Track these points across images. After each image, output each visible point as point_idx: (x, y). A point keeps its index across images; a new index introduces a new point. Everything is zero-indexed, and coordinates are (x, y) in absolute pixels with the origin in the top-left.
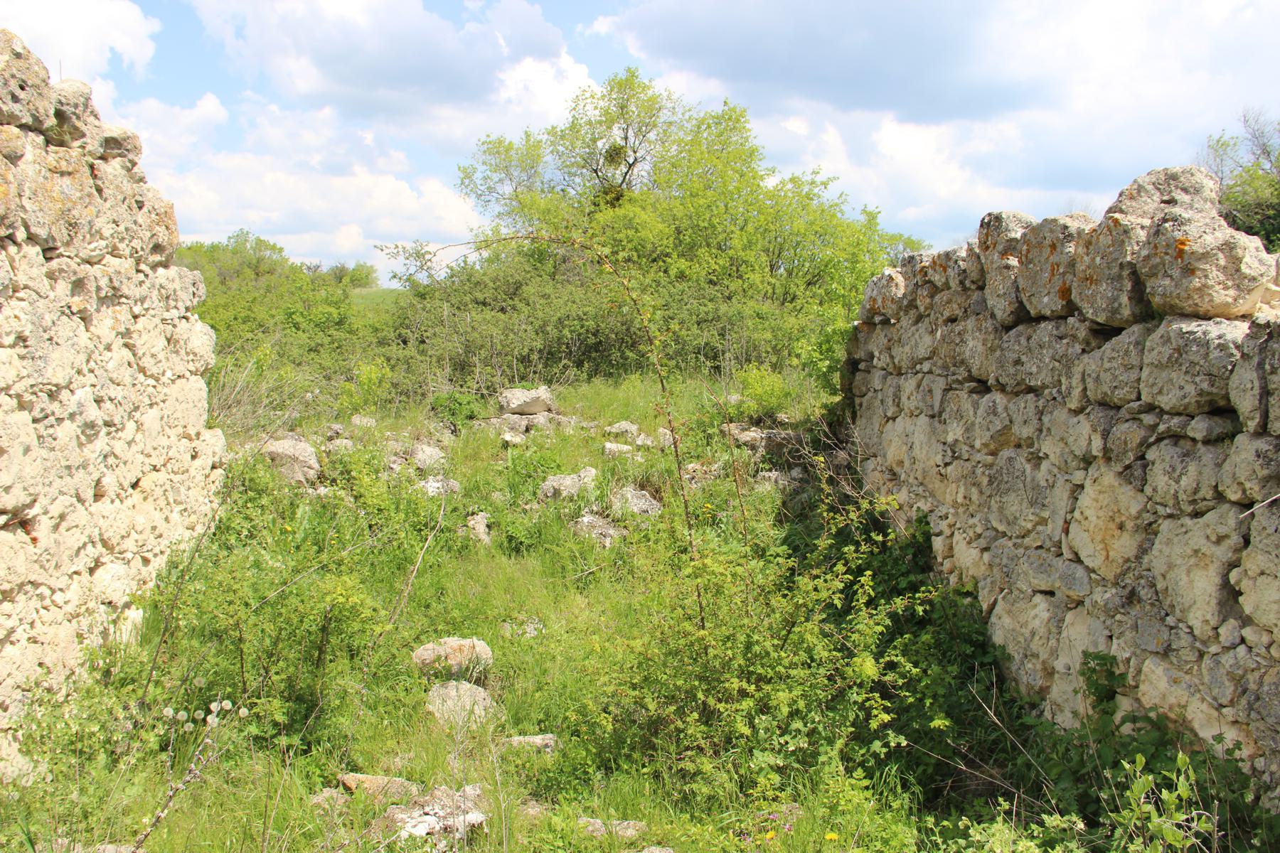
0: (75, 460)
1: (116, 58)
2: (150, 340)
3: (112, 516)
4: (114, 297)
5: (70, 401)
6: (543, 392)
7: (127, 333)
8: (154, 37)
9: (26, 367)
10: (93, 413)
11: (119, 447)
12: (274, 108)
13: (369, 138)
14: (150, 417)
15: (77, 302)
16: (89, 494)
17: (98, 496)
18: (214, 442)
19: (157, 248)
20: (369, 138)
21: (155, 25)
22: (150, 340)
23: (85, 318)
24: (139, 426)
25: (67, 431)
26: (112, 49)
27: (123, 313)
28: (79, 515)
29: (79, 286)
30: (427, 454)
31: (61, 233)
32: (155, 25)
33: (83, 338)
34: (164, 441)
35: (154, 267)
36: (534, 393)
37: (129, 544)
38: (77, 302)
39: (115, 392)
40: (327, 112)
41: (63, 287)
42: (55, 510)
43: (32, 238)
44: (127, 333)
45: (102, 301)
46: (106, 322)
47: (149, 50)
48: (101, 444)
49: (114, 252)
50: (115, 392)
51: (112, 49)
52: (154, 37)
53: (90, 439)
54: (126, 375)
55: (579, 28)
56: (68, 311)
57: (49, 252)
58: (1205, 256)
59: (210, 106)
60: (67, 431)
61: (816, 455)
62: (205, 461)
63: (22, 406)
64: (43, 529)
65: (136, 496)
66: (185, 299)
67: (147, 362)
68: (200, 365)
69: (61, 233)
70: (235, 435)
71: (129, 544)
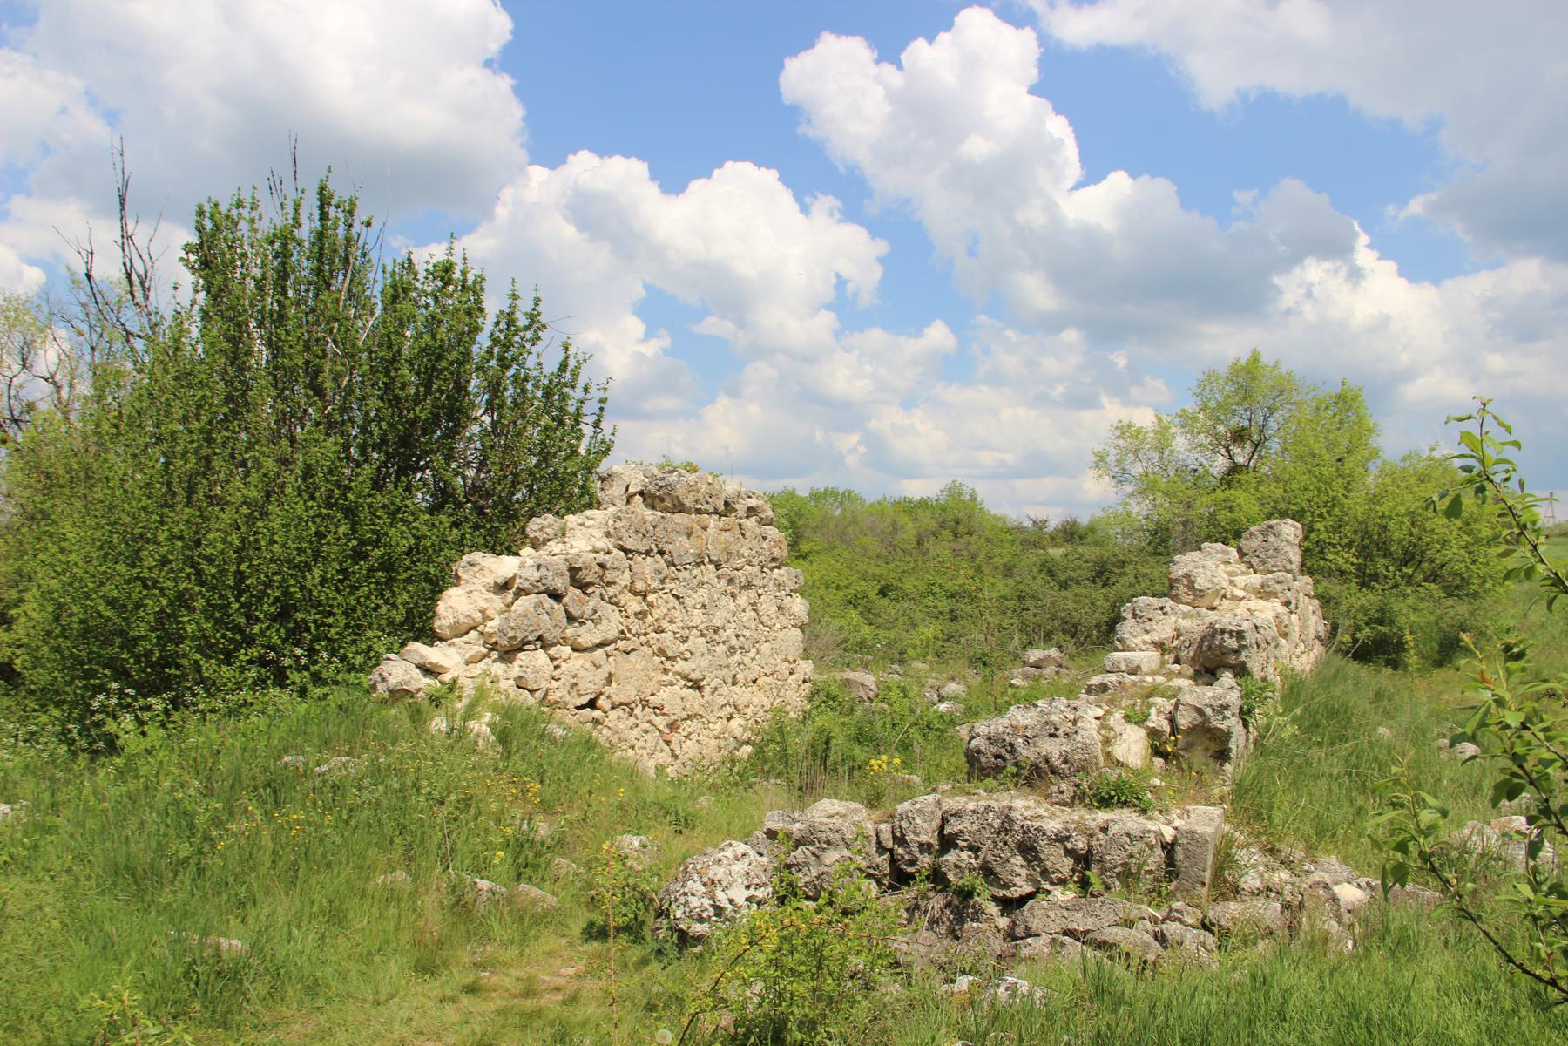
0: (724, 663)
1: (841, 283)
2: (768, 607)
3: (741, 694)
4: (748, 586)
5: (724, 635)
6: (1054, 652)
7: (755, 604)
8: (881, 261)
9: (704, 618)
10: (734, 642)
11: (746, 660)
12: (1010, 333)
13: (1121, 361)
14: (765, 647)
15: (729, 589)
16: (730, 681)
17: (734, 684)
18: (806, 667)
19: (774, 559)
20: (1121, 361)
21: (882, 247)
22: (768, 607)
23: (733, 596)
24: (758, 652)
25: (721, 649)
26: (838, 276)
27: (752, 594)
28: (724, 690)
29: (731, 581)
30: (952, 688)
31: (723, 557)
32: (882, 247)
33: (732, 606)
34: (773, 661)
35: (772, 569)
36: (1046, 653)
37: (749, 711)
38: (729, 589)
39: (746, 632)
40: (1071, 336)
41: (723, 582)
42: (713, 684)
43: (711, 561)
44: (755, 604)
45: (742, 588)
46: (743, 599)
47: (877, 272)
48: (737, 657)
49: (750, 563)
50: (746, 632)
51: (838, 276)
52: (881, 261)
53: (733, 654)
54: (753, 625)
55: (1390, 210)
56: (725, 593)
57: (718, 566)
58: (1176, 580)
59: (938, 335)
60: (721, 649)
61: (1306, 709)
62: (799, 676)
63: (702, 635)
64: (707, 690)
65: (755, 688)
66: (791, 585)
67: (765, 619)
68: (799, 622)
69: (723, 557)
70: (819, 662)
71: (749, 711)
